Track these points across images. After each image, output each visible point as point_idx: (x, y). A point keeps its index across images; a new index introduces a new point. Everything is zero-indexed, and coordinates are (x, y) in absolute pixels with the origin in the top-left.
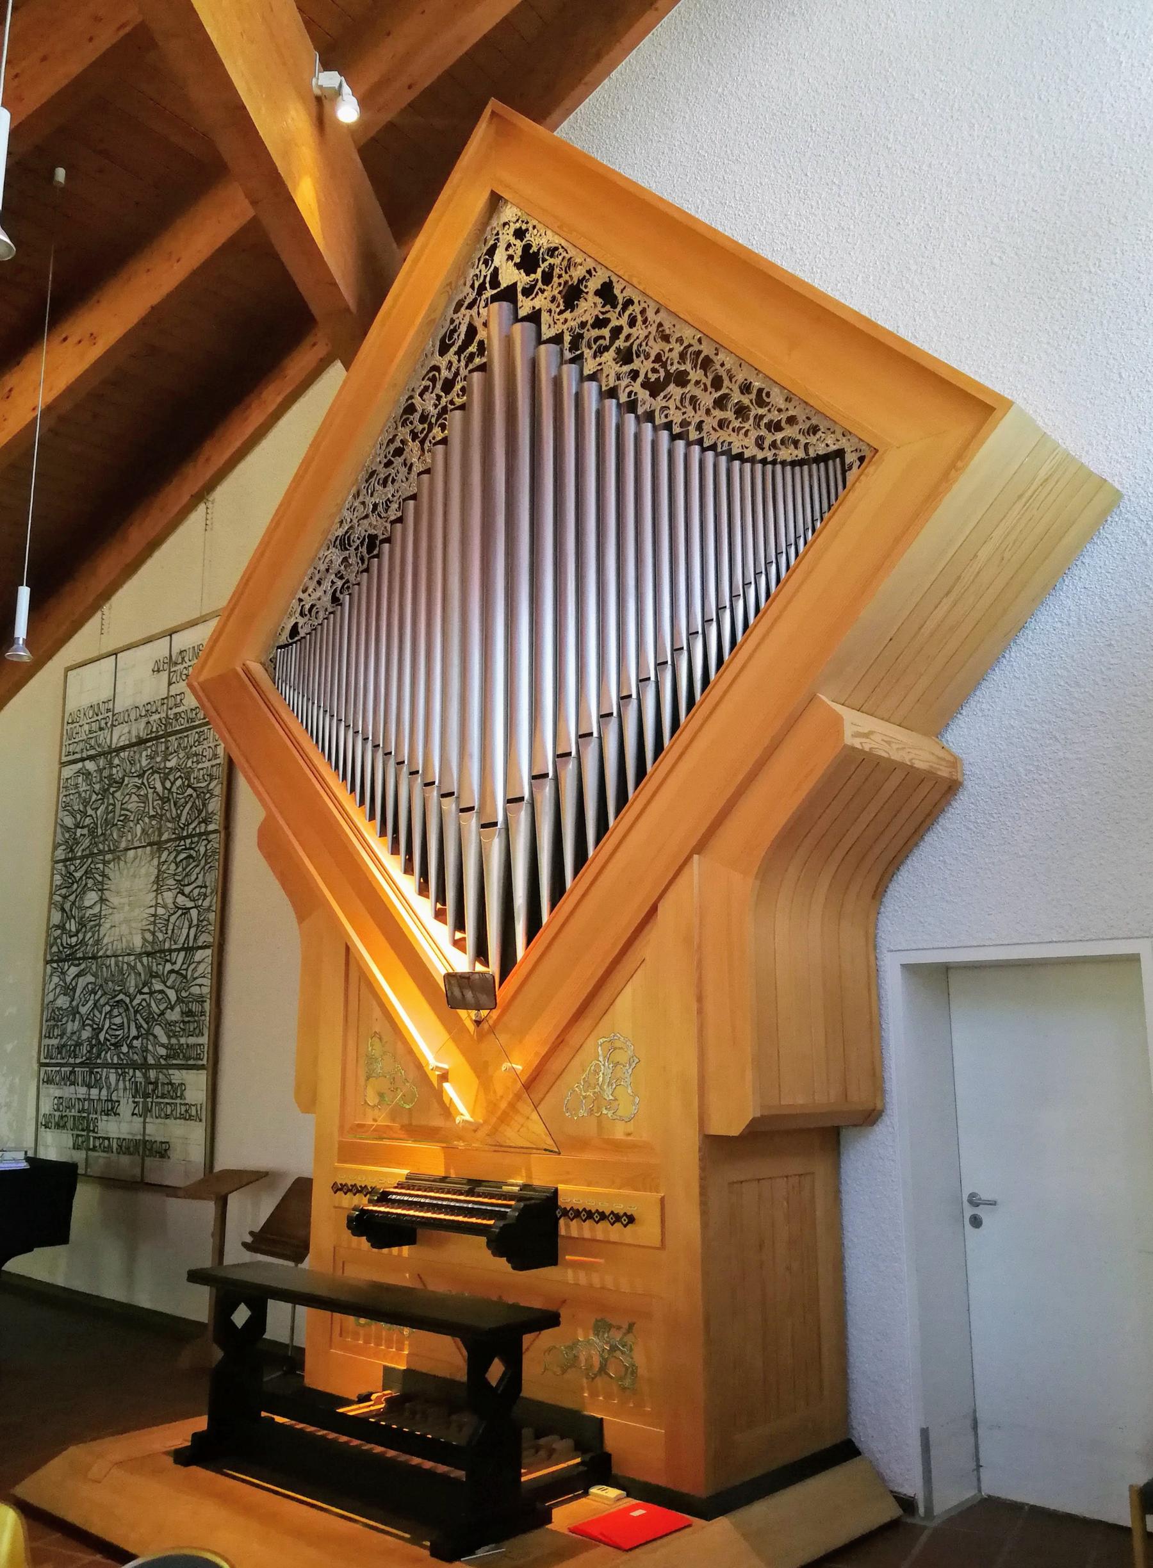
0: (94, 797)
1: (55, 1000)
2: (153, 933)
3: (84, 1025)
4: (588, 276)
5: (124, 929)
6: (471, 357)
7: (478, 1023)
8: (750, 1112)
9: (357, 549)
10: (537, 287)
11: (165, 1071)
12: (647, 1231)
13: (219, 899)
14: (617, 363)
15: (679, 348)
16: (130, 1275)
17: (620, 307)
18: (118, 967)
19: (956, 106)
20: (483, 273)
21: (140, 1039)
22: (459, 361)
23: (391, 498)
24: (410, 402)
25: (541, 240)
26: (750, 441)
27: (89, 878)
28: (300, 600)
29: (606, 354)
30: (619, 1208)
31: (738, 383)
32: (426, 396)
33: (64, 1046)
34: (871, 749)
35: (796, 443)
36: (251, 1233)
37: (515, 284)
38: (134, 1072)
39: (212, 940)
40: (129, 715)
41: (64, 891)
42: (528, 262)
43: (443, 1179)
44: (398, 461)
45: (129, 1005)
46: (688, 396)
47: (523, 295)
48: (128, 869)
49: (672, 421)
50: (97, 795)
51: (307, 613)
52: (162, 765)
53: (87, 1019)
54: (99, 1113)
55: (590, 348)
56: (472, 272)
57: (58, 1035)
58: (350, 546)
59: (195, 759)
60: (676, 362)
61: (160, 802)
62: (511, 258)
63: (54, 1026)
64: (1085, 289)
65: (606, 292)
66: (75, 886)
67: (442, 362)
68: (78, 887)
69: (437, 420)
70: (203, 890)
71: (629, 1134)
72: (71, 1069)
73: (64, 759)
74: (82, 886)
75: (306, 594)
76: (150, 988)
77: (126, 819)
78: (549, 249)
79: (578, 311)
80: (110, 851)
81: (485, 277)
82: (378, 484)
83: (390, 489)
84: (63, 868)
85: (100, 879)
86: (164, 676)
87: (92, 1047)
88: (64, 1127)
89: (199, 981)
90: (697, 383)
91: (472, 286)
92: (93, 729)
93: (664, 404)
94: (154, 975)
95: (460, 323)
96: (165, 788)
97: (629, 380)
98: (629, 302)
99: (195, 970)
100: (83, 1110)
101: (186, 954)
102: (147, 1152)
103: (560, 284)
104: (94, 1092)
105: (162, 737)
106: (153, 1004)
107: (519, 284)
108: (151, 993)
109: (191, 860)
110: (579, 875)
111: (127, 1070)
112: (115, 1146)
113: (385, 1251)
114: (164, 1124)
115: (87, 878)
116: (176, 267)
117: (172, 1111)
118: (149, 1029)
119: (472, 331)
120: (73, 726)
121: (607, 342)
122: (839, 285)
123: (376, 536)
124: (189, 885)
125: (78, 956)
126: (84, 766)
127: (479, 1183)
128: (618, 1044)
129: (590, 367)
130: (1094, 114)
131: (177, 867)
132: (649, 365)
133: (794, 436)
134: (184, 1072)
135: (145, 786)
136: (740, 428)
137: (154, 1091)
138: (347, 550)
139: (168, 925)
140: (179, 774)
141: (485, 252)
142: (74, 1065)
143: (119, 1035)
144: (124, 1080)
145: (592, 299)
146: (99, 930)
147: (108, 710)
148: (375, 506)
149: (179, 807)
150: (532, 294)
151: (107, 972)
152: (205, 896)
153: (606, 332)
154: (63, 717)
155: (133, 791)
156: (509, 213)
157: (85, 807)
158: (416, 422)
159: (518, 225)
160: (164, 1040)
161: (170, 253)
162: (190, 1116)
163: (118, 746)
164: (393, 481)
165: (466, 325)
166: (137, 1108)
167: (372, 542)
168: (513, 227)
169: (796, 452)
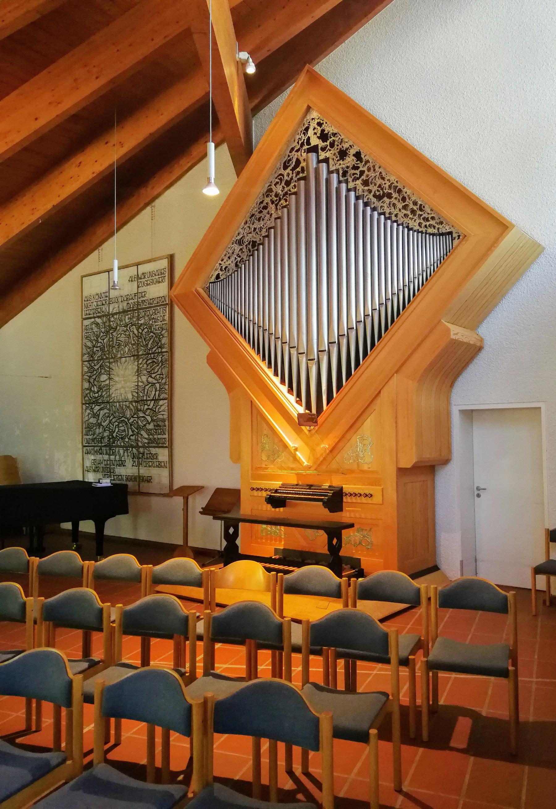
0: (102, 334)
1: (88, 420)
2: (137, 393)
3: (105, 430)
4: (350, 148)
5: (122, 391)
6: (298, 173)
7: (310, 431)
8: (414, 460)
9: (246, 246)
10: (327, 148)
11: (147, 449)
12: (377, 498)
13: (170, 379)
14: (362, 185)
15: (388, 184)
16: (135, 528)
17: (364, 163)
18: (121, 407)
19: (491, 85)
20: (303, 138)
21: (134, 436)
22: (293, 174)
23: (262, 227)
24: (270, 187)
25: (329, 129)
26: (416, 224)
27: (103, 369)
28: (220, 264)
29: (357, 181)
30: (367, 492)
31: (412, 200)
32: (278, 186)
33: (95, 438)
34: (458, 339)
35: (434, 227)
36: (202, 508)
37: (318, 145)
38: (132, 449)
39: (167, 396)
40: (118, 300)
41: (89, 374)
42: (324, 137)
43: (297, 485)
44: (265, 212)
45: (128, 422)
46: (392, 203)
47: (321, 150)
48: (123, 366)
49: (385, 212)
50: (103, 333)
51: (224, 270)
52: (137, 322)
53: (106, 427)
54: (115, 465)
55: (351, 177)
56: (298, 137)
57: (92, 434)
58: (244, 244)
59: (153, 321)
60: (387, 189)
61: (136, 338)
62: (315, 134)
63: (90, 430)
64: (536, 168)
65: (358, 155)
66: (95, 372)
67: (285, 173)
68: (96, 373)
69: (283, 197)
70: (161, 376)
71: (369, 468)
72: (99, 448)
73: (84, 317)
74: (98, 372)
75: (223, 262)
76: (137, 416)
77: (119, 345)
78: (333, 133)
79: (345, 161)
80: (112, 358)
81: (304, 140)
82: (256, 220)
83: (262, 223)
84: (88, 364)
85: (108, 369)
86: (135, 284)
87: (110, 439)
88: (98, 471)
89: (162, 413)
90: (396, 198)
91: (298, 143)
92: (99, 304)
93: (382, 204)
94: (139, 410)
95: (293, 158)
96: (139, 332)
97: (368, 193)
98: (367, 162)
99: (160, 408)
100: (107, 464)
101: (154, 402)
102: (141, 481)
103: (338, 149)
104: (112, 457)
105: (135, 310)
106: (139, 422)
107: (319, 145)
108: (138, 418)
109: (155, 363)
110: (349, 380)
111: (128, 448)
112: (124, 478)
113: (277, 509)
114: (149, 469)
115: (101, 369)
116: (161, 117)
117: (152, 464)
118: (138, 432)
119: (298, 162)
120: (88, 302)
121: (358, 176)
122: (443, 152)
123: (256, 242)
124: (154, 373)
125: (99, 402)
126: (95, 320)
127: (312, 486)
128: (365, 438)
129: (351, 185)
130: (543, 100)
131: (147, 366)
132: (376, 188)
133: (433, 224)
134: (157, 449)
135: (128, 331)
136: (412, 218)
137: (142, 456)
138: (242, 245)
139: (144, 390)
140: (145, 327)
141: (304, 129)
142: (101, 447)
143: (123, 435)
144: (127, 453)
145: (351, 156)
146: (109, 391)
147: (106, 297)
148: (255, 229)
149: (147, 341)
150: (325, 151)
151: (115, 409)
152: (163, 378)
153: (358, 172)
154: (82, 299)
155: (123, 332)
156: (314, 114)
157: (97, 338)
158: (273, 196)
159: (319, 121)
160: (147, 436)
161: (158, 111)
162: (161, 466)
163: (113, 312)
164: (263, 220)
165: (295, 159)
166: (135, 463)
167: (254, 244)
168: (316, 121)
169: (434, 230)
